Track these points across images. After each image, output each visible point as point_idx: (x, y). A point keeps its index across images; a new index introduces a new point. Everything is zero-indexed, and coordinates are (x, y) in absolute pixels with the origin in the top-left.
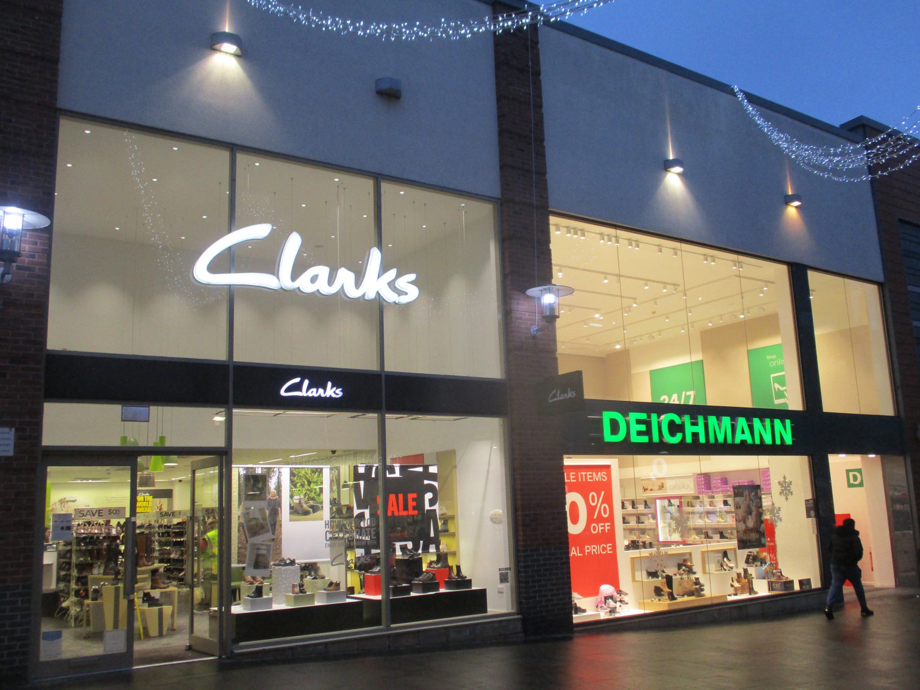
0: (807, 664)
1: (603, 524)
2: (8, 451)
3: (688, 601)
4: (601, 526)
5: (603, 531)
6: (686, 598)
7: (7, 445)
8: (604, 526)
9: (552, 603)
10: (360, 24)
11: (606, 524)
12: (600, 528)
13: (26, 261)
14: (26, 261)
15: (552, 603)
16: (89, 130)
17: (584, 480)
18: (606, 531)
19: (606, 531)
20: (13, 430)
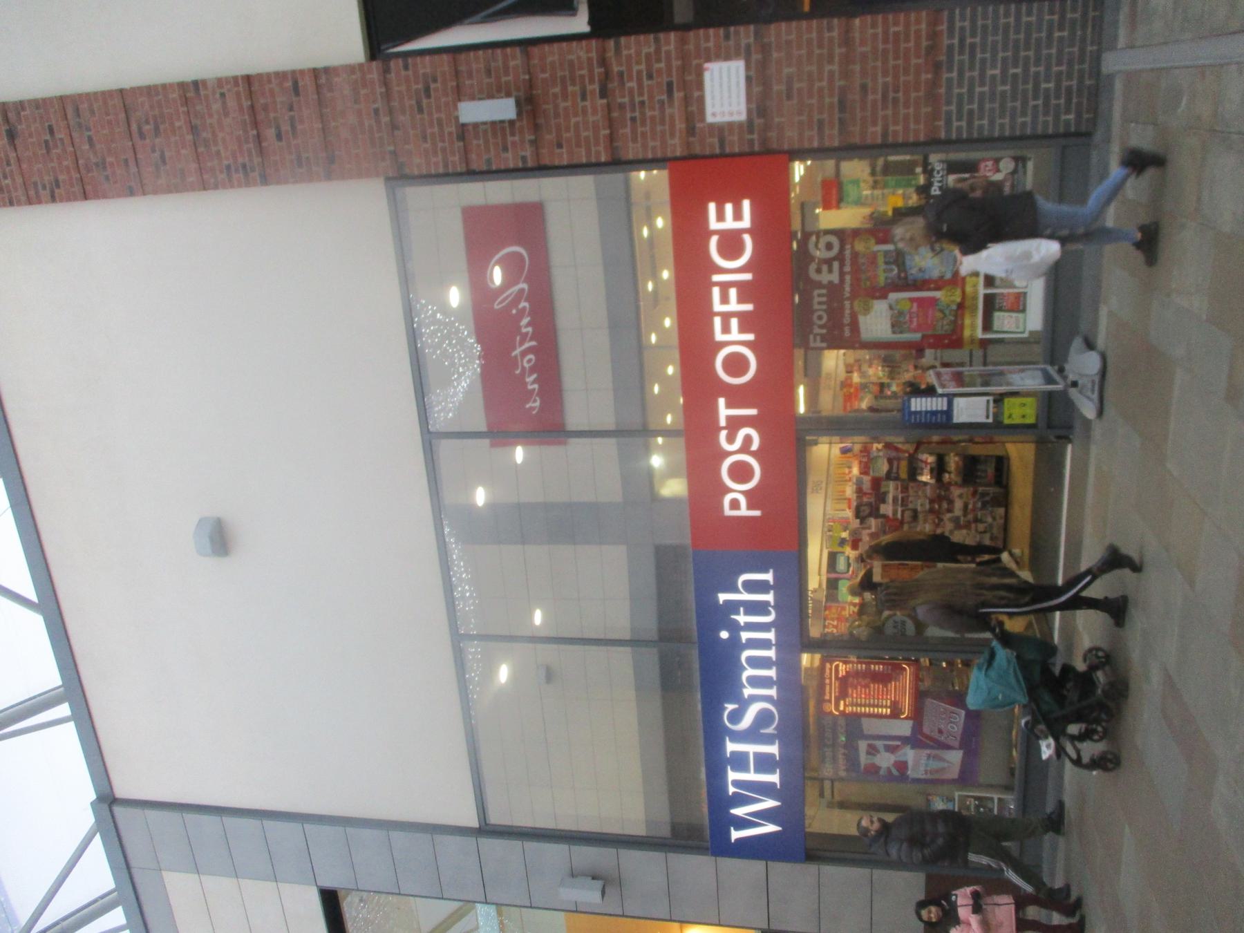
0: (943, 801)
1: (717, 321)
2: (737, 69)
3: (992, 370)
4: (726, 329)
5: (747, 322)
6: (955, 438)
7: (720, 72)
8: (726, 317)
9: (968, 33)
10: (652, 227)
11: (718, 307)
12: (735, 335)
13: (940, 91)
14: (940, 91)
15: (968, 33)
16: (650, 335)
17: (969, 9)
18: (748, 307)
19: (748, 307)
20: (706, 65)
